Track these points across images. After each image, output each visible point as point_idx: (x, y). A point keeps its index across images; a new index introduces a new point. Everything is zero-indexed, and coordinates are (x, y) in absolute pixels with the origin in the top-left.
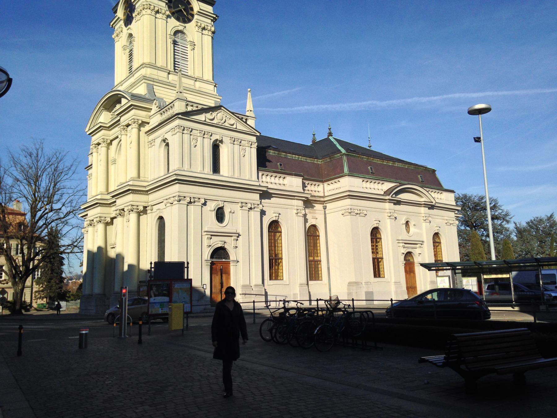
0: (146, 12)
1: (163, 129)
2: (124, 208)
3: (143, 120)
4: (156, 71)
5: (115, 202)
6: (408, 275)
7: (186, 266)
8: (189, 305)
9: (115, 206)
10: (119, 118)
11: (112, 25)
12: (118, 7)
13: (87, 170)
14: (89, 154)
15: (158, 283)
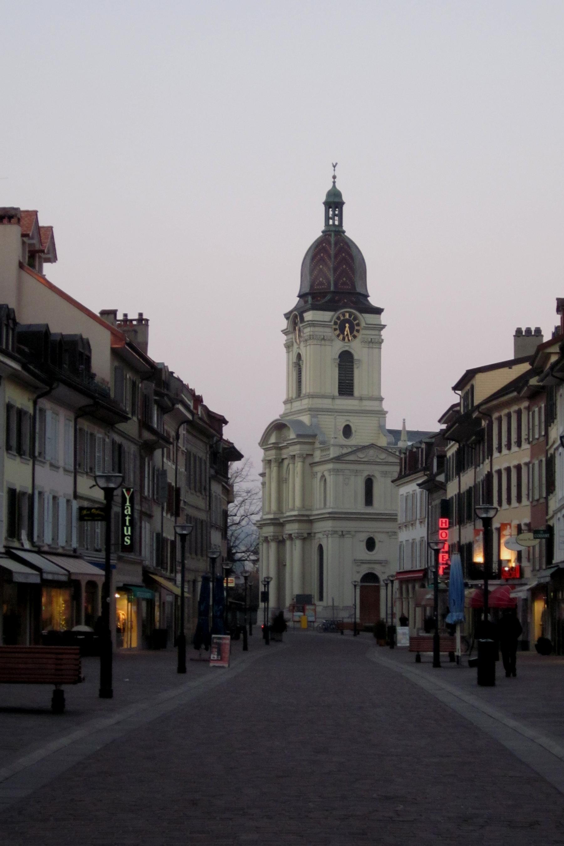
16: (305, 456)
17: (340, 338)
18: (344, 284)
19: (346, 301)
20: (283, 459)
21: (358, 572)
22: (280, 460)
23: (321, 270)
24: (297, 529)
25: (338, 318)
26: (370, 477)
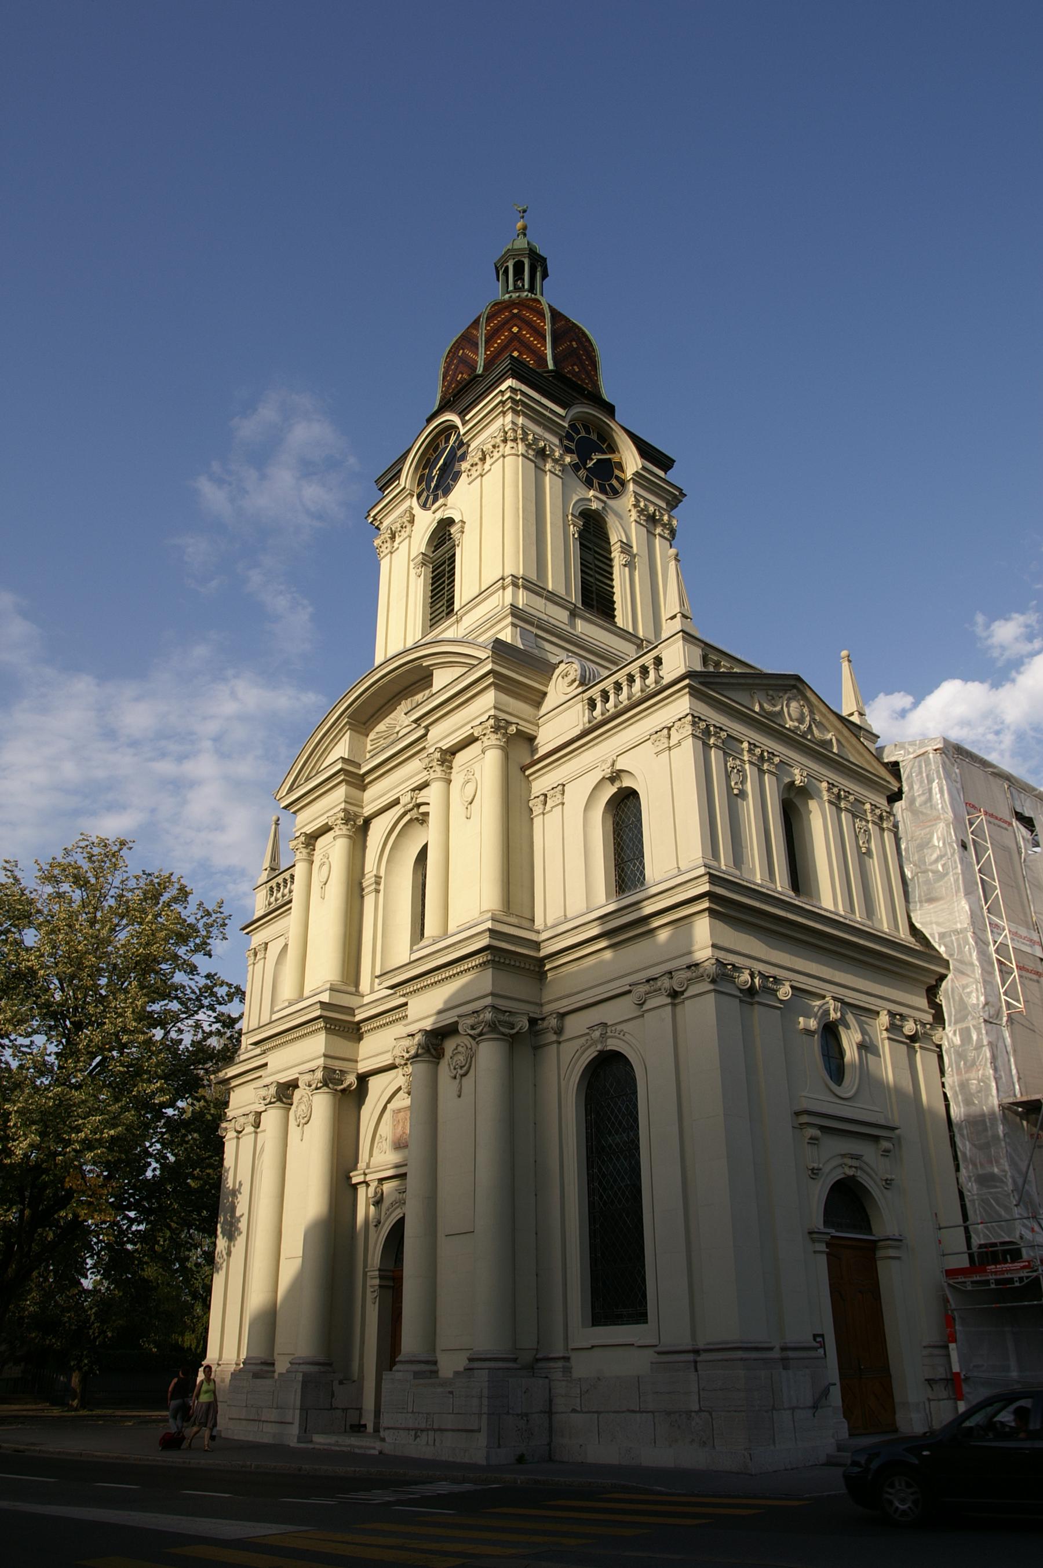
0: (513, 448)
1: (596, 748)
2: (297, 1079)
5: (406, 1004)
6: (209, 1283)
9: (404, 1022)
10: (422, 732)
12: (404, 463)
13: (247, 933)
14: (259, 883)
22: (360, 822)
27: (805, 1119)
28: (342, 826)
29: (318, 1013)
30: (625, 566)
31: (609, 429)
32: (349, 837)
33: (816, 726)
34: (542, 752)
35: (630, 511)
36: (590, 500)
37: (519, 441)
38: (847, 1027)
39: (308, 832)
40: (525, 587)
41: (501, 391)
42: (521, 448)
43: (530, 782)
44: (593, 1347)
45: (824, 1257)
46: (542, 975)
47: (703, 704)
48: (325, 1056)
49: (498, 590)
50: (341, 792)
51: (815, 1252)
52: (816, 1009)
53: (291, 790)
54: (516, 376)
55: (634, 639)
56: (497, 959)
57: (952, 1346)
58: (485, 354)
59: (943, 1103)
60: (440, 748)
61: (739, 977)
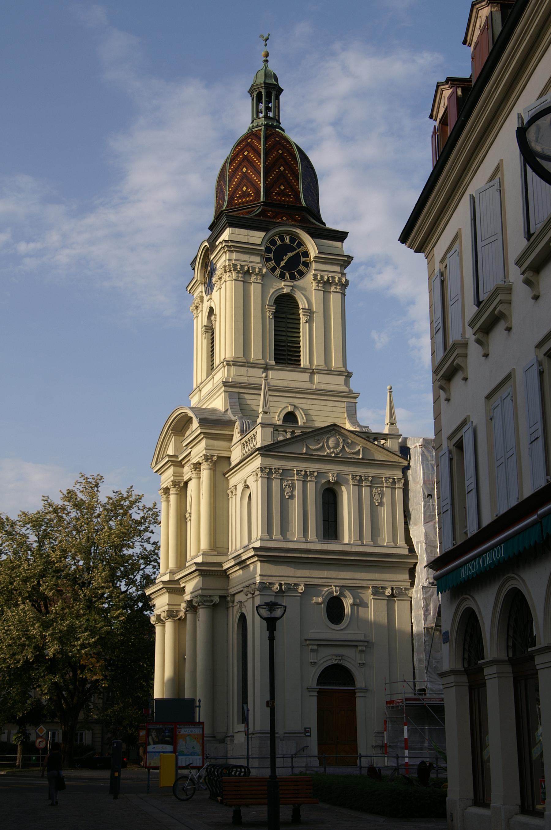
2: (160, 615)
3: (219, 455)
4: (246, 369)
7: (198, 704)
8: (201, 757)
11: (189, 291)
15: (158, 727)
16: (215, 458)
17: (276, 273)
18: (282, 193)
19: (280, 152)
20: (186, 483)
21: (314, 664)
22: (182, 485)
23: (245, 175)
24: (201, 589)
25: (273, 242)
26: (331, 486)
27: (308, 642)
28: (173, 489)
29: (161, 586)
30: (306, 322)
31: (296, 234)
32: (210, 469)
33: (347, 446)
34: (233, 464)
35: (312, 283)
36: (283, 288)
37: (233, 271)
38: (346, 597)
39: (164, 487)
40: (234, 365)
41: (220, 242)
42: (234, 274)
43: (228, 480)
44: (238, 732)
45: (316, 698)
46: (228, 577)
47: (270, 459)
48: (168, 604)
49: (221, 368)
50: (171, 471)
51: (310, 696)
52: (323, 593)
53: (156, 464)
54: (232, 224)
55: (308, 371)
56: (203, 573)
57: (385, 732)
58: (229, 191)
59: (410, 625)
60: (193, 463)
61: (273, 587)
